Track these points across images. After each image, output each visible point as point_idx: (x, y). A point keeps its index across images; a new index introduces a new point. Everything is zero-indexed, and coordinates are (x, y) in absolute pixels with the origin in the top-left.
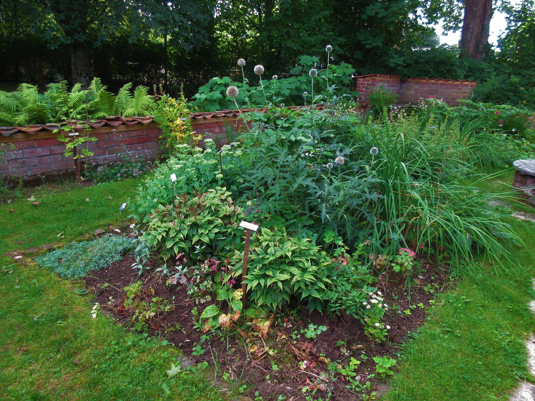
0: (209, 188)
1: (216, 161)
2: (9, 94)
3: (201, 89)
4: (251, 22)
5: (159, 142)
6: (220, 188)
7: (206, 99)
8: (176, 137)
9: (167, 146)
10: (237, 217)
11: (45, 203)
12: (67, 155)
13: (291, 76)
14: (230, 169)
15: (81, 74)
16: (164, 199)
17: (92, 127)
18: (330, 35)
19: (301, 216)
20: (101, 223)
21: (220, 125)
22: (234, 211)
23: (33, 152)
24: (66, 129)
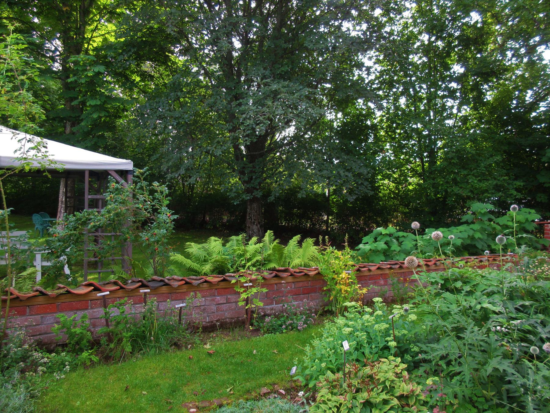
0: (380, 357)
1: (388, 326)
2: (200, 246)
3: (365, 239)
4: (412, 170)
5: (323, 293)
6: (394, 358)
7: (370, 250)
8: (341, 290)
9: (331, 299)
10: (416, 398)
11: (218, 353)
12: (241, 304)
13: (460, 224)
14: (404, 335)
15: (254, 223)
16: (332, 364)
17: (264, 278)
18: (504, 180)
19: (497, 407)
20: (267, 381)
21: (385, 277)
22: (412, 391)
23: (213, 300)
24: (243, 280)
